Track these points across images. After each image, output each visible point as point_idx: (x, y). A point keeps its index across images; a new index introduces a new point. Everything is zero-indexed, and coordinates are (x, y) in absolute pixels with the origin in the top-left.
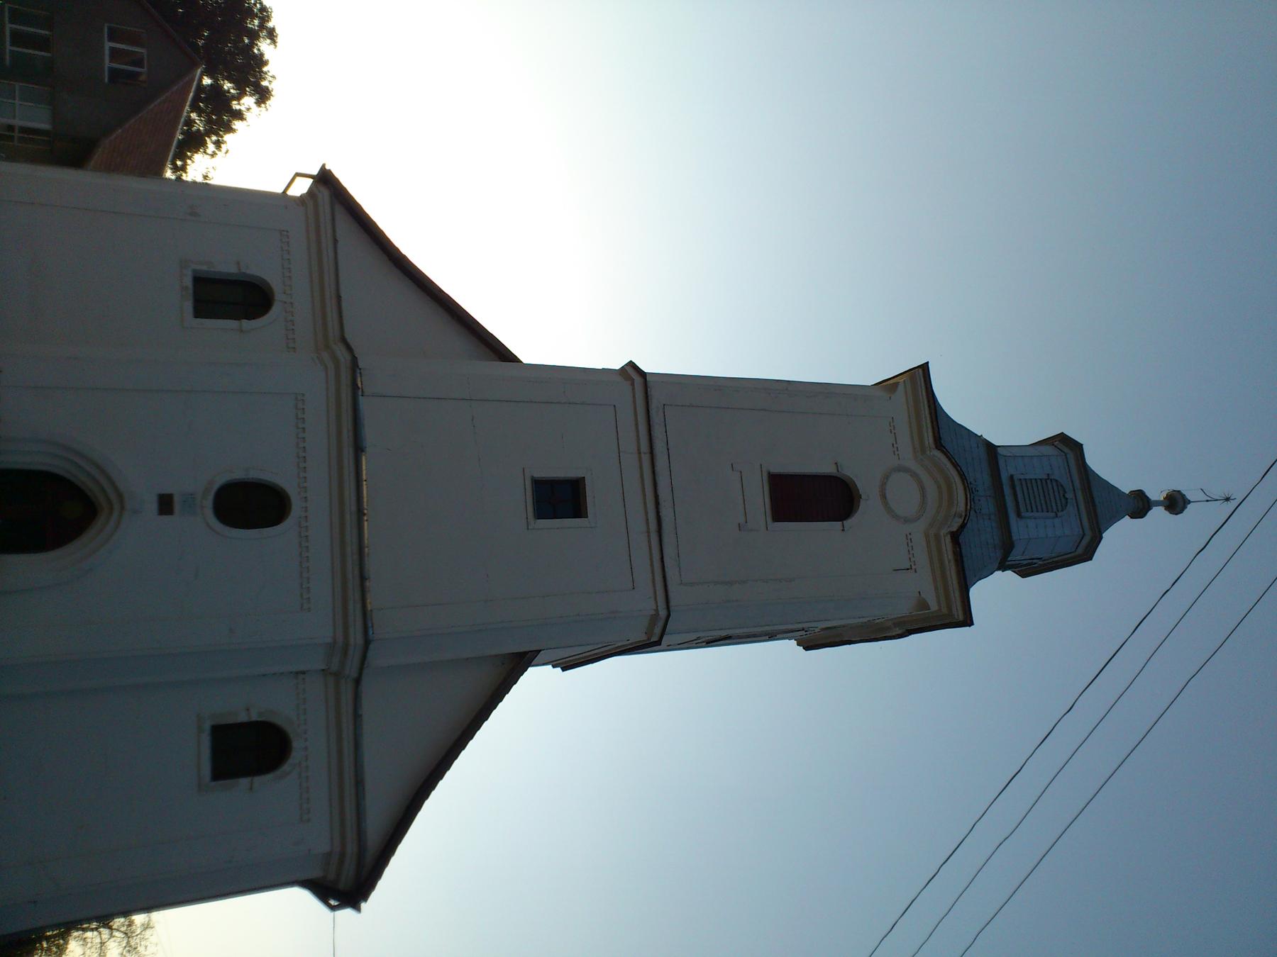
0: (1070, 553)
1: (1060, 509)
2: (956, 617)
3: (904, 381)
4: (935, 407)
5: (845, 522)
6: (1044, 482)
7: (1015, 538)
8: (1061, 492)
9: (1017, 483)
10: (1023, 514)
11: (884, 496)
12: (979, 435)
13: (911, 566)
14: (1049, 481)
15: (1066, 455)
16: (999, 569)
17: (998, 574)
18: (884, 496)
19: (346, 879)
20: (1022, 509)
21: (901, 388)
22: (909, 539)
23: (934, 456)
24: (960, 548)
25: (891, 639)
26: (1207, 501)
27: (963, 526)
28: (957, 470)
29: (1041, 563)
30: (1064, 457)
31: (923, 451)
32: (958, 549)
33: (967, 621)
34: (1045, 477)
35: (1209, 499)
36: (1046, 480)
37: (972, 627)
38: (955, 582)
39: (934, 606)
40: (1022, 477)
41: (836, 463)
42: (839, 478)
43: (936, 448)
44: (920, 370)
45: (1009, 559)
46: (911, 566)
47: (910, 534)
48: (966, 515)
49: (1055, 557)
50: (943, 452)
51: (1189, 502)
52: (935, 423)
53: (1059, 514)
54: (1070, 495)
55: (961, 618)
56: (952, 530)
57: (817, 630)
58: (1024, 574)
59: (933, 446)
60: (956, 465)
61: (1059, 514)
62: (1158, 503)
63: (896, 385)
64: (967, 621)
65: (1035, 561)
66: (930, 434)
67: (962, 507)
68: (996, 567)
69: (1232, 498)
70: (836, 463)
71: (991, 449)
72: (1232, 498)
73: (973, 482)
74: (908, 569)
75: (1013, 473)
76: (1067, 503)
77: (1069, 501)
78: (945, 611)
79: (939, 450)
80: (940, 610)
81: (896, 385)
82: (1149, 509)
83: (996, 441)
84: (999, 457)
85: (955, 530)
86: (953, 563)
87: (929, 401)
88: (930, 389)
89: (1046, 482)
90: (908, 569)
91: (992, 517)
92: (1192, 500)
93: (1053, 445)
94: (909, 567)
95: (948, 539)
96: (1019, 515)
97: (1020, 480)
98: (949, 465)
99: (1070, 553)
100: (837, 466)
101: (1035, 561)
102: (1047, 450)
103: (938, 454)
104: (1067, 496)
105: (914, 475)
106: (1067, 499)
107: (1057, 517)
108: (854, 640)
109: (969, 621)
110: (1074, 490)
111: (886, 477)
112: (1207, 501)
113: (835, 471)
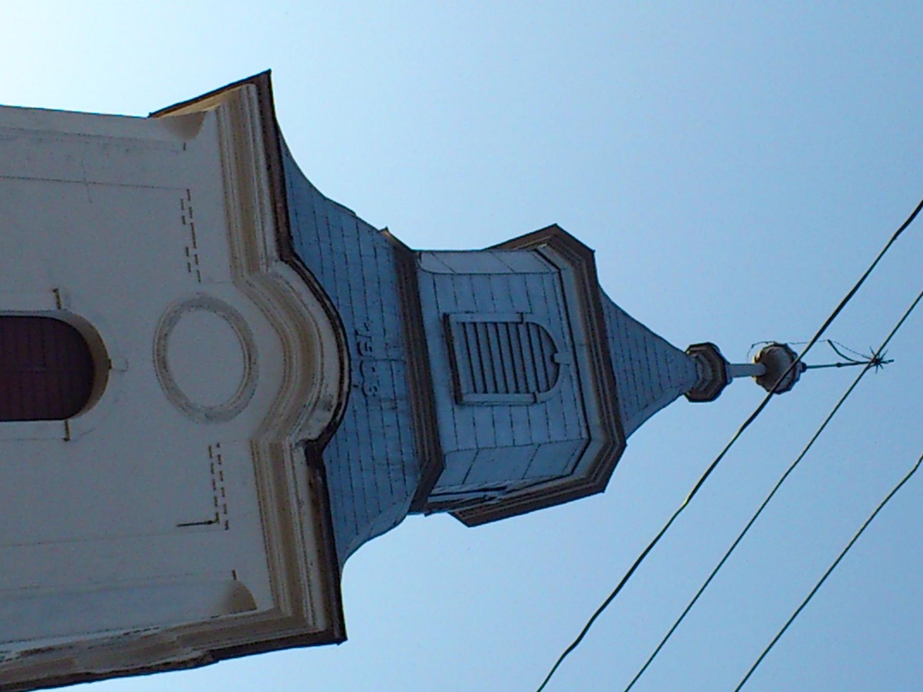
0: (561, 477)
1: (543, 386)
2: (310, 622)
3: (217, 112)
4: (278, 140)
5: (70, 421)
6: (512, 329)
7: (448, 445)
8: (547, 351)
9: (456, 333)
10: (465, 398)
11: (162, 364)
12: (379, 228)
13: (217, 514)
14: (522, 328)
15: (560, 273)
16: (413, 510)
17: (414, 522)
18: (162, 364)
19: (694, 396)
20: (465, 386)
21: (209, 123)
22: (215, 458)
23: (276, 275)
24: (324, 478)
25: (179, 669)
26: (839, 365)
27: (331, 429)
28: (324, 306)
29: (503, 497)
30: (556, 275)
31: (253, 266)
32: (320, 479)
33: (342, 638)
34: (517, 319)
35: (844, 361)
36: (517, 324)
37: (344, 644)
38: (312, 555)
39: (264, 602)
40: (467, 318)
41: (55, 291)
42: (70, 326)
43: (281, 258)
44: (253, 88)
45: (435, 491)
46: (217, 514)
47: (218, 446)
48: (339, 405)
49: (530, 486)
50: (295, 267)
51: (805, 367)
52: (279, 205)
53: (541, 396)
54: (565, 357)
55: (321, 625)
56: (310, 437)
57: (13, 655)
58: (471, 520)
59: (275, 255)
60: (320, 296)
61: (541, 396)
62: (743, 370)
63: (199, 117)
64: (342, 638)
65: (490, 494)
66: (269, 227)
67: (332, 389)
68: (406, 511)
69: (885, 359)
70: (55, 291)
71: (399, 249)
72: (885, 359)
73: (362, 331)
74: (210, 522)
75: (447, 311)
76: (557, 374)
77: (562, 368)
78: (287, 611)
79: (287, 262)
80: (278, 608)
81: (199, 117)
82: (725, 382)
83: (413, 244)
84: (420, 274)
85: (314, 436)
86: (307, 508)
87: (268, 157)
88: (269, 114)
89: (517, 329)
90: (210, 522)
91: (401, 405)
92: (808, 364)
93: (536, 250)
94: (213, 518)
95: (300, 456)
96: (457, 399)
97: (464, 324)
98: (308, 297)
99: (561, 477)
100: (58, 297)
101: (490, 494)
102: (524, 261)
103: (284, 271)
104: (557, 358)
105: (233, 317)
106: (558, 365)
107: (535, 402)
108: (98, 671)
109: (337, 635)
110: (573, 347)
111: (171, 320)
112: (839, 365)
113: (53, 308)
